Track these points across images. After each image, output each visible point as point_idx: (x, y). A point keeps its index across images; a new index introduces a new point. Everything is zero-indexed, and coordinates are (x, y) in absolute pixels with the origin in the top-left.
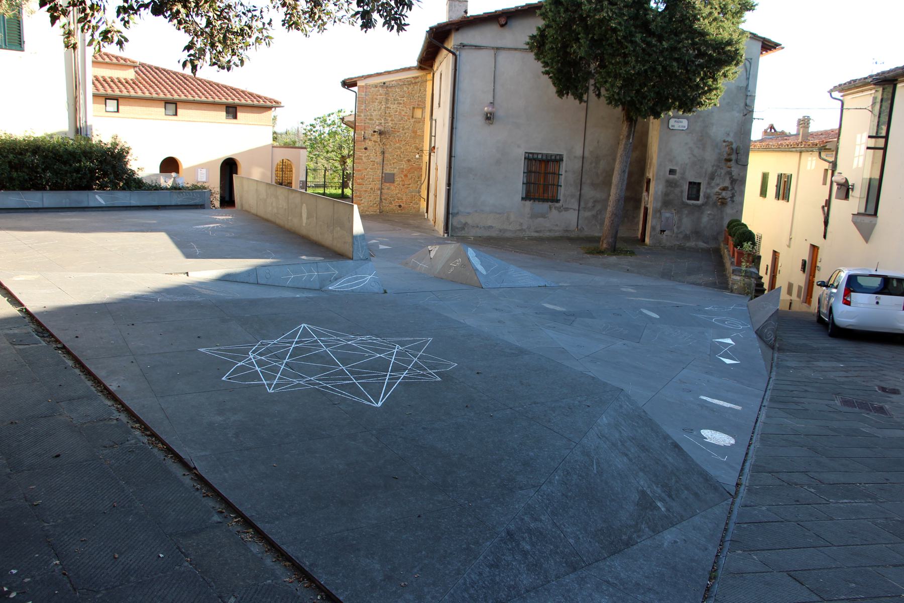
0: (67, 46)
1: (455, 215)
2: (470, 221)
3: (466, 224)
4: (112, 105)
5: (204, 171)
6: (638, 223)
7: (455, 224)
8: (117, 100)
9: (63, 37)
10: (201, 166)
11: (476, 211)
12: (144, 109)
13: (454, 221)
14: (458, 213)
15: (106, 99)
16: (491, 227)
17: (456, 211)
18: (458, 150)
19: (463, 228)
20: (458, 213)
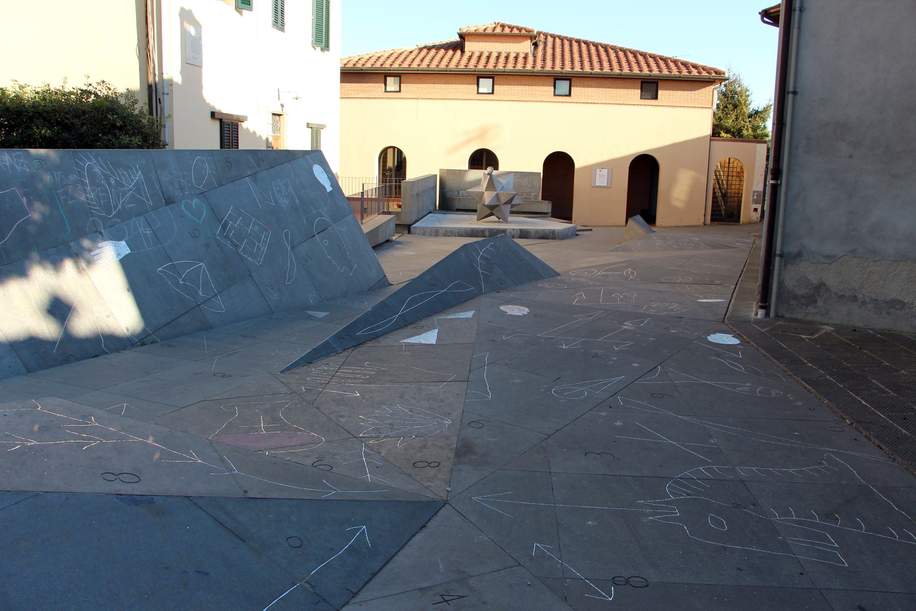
0: (103, 82)
1: (791, 258)
2: (832, 281)
3: (821, 287)
4: (563, 86)
5: (605, 172)
6: (712, 303)
7: (790, 283)
8: (570, 80)
9: (42, 85)
10: (601, 165)
11: (853, 252)
12: (526, 88)
13: (789, 277)
14: (799, 255)
15: (555, 80)
16: (896, 304)
17: (793, 248)
18: (808, 71)
19: (811, 300)
20: (799, 255)
